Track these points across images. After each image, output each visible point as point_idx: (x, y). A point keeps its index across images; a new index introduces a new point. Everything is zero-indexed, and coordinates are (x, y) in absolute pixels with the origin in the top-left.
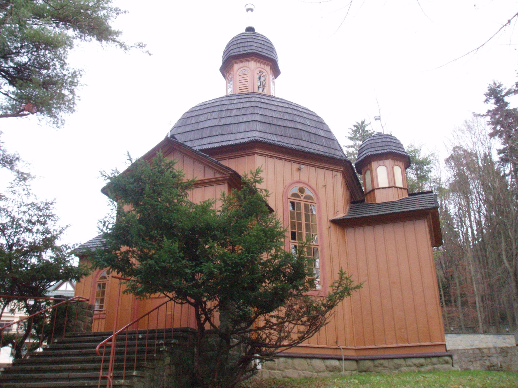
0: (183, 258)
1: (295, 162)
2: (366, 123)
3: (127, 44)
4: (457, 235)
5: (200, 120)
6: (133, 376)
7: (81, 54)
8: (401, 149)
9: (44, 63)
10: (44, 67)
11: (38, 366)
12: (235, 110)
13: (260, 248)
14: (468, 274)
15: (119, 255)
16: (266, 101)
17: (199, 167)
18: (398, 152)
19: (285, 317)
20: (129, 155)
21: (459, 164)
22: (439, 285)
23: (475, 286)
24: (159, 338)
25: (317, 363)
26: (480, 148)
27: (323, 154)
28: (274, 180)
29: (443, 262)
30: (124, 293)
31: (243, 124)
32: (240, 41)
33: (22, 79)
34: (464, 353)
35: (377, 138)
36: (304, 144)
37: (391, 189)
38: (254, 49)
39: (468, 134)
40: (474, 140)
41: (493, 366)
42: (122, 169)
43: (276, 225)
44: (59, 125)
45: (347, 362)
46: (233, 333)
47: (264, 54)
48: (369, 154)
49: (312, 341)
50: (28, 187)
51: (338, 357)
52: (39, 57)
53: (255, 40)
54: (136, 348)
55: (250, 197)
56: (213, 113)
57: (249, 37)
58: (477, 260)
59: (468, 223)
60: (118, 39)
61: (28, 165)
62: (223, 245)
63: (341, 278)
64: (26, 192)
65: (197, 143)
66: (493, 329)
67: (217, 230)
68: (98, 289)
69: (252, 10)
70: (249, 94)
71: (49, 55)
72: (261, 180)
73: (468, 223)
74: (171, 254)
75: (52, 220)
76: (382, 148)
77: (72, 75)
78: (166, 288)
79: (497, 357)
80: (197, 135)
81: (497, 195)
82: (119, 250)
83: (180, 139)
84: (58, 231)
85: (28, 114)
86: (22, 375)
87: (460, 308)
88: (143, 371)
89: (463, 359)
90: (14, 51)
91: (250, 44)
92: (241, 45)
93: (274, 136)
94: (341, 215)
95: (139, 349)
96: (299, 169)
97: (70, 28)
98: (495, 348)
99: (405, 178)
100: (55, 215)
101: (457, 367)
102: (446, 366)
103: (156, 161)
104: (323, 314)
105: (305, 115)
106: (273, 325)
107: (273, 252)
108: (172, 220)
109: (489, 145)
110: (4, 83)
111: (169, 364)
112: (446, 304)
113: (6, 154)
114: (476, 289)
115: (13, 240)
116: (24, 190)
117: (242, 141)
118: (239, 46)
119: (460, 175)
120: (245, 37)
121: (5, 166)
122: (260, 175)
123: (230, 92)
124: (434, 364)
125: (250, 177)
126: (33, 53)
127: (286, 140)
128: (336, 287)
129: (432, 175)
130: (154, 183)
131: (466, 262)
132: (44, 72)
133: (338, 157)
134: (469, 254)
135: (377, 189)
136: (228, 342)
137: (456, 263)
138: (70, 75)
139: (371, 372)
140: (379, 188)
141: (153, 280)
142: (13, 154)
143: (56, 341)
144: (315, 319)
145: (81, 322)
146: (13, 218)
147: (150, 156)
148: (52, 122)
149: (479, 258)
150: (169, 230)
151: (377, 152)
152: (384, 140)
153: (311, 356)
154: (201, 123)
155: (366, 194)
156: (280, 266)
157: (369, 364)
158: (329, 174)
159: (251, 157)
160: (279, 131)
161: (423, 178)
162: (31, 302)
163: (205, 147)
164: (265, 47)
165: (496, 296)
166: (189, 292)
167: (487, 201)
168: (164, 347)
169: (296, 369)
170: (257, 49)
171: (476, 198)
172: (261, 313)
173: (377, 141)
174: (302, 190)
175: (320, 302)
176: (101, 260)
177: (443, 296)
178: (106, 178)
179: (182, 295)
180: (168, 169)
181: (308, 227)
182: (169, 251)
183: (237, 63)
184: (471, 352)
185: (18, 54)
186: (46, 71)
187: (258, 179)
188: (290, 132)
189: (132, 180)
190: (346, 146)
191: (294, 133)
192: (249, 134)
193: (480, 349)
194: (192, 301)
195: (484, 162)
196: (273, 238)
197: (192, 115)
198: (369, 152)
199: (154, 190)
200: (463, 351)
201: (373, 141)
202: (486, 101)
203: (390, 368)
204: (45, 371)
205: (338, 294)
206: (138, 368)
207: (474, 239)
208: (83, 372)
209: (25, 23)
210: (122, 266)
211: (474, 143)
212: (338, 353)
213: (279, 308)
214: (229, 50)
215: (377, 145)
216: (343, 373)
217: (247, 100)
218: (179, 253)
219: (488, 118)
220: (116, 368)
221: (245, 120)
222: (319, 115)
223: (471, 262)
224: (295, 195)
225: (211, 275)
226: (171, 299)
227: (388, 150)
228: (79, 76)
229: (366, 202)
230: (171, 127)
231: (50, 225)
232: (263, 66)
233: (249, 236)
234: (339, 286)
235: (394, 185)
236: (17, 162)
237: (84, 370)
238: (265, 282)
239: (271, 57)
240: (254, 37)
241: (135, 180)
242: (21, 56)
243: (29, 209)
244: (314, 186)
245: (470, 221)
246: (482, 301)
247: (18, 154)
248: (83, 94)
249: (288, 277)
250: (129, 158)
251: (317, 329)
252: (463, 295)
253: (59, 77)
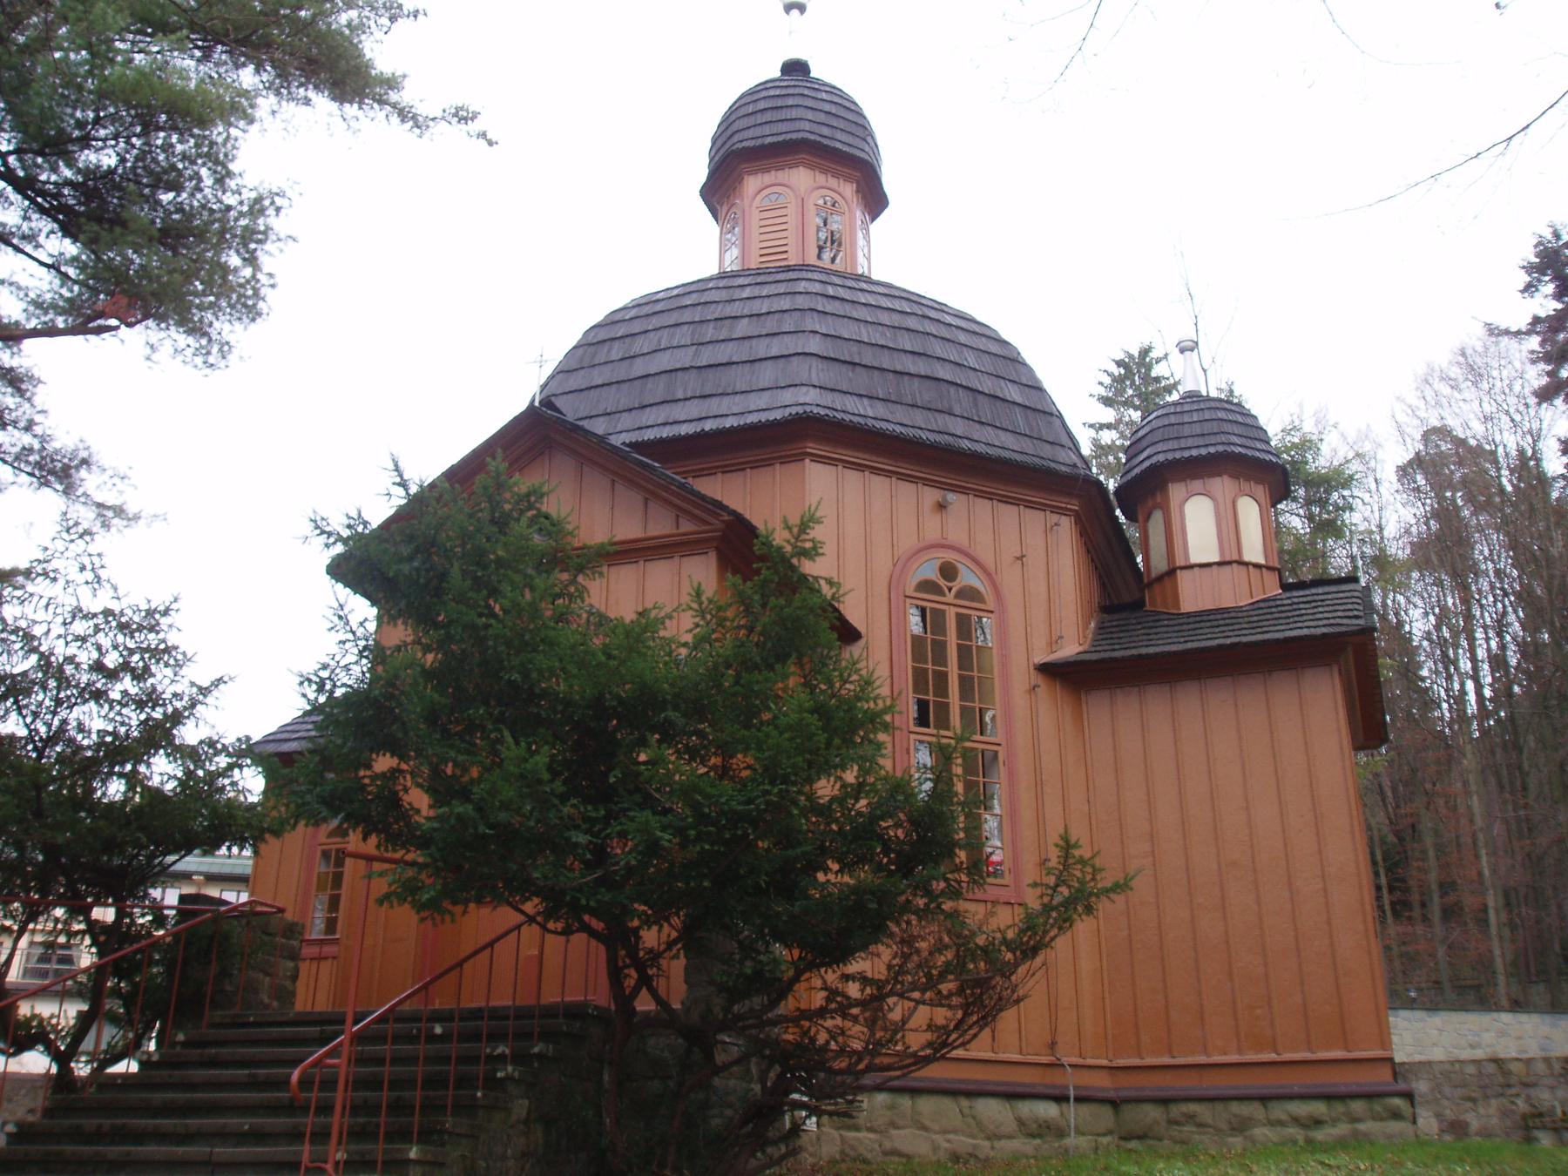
0: (564, 798)
2: (1154, 354)
3: (422, 110)
4: (1432, 704)
5: (636, 349)
6: (410, 1161)
7: (281, 145)
8: (1259, 445)
9: (165, 172)
10: (167, 182)
11: (118, 1122)
12: (746, 320)
13: (810, 767)
14: (1463, 821)
15: (367, 781)
16: (842, 293)
17: (630, 499)
18: (1250, 453)
19: (887, 982)
20: (397, 469)
21: (1439, 484)
22: (1372, 854)
23: (1484, 859)
24: (496, 1037)
25: (991, 1109)
26: (1506, 434)
27: (1018, 457)
28: (858, 536)
29: (1386, 783)
30: (380, 902)
31: (769, 363)
32: (762, 105)
33: (99, 220)
34: (1450, 1074)
35: (1186, 408)
36: (958, 427)
37: (1227, 569)
38: (805, 129)
39: (1470, 393)
40: (1487, 408)
41: (1541, 1115)
42: (378, 513)
43: (862, 690)
44: (211, 360)
45: (1086, 1110)
46: (723, 1027)
47: (838, 145)
48: (1161, 458)
49: (980, 1048)
50: (96, 560)
51: (1057, 1092)
52: (150, 152)
53: (810, 103)
54: (420, 1070)
55: (782, 601)
56: (678, 330)
57: (791, 91)
58: (1492, 780)
59: (1465, 665)
60: (393, 96)
61: (116, 480)
62: (693, 754)
63: (1066, 866)
64: (89, 576)
65: (626, 421)
66: (1539, 992)
67: (676, 708)
68: (321, 867)
69: (802, 8)
70: (789, 269)
71: (179, 148)
72: (815, 548)
73: (1465, 665)
74: (528, 786)
75: (167, 665)
76: (1201, 441)
77: (251, 207)
78: (514, 888)
79: (1552, 1088)
80: (623, 397)
81: (1556, 582)
82: (369, 767)
83: (570, 409)
84: (186, 698)
85: (116, 328)
86: (69, 1149)
87: (1438, 929)
88: (443, 1145)
89: (1447, 1090)
90: (76, 133)
91: (794, 113)
92: (768, 116)
93: (866, 401)
94: (1070, 649)
95: (433, 1066)
96: (941, 507)
97: (244, 65)
98: (1547, 1060)
99: (1273, 532)
100: (176, 648)
101: (1427, 1122)
102: (1394, 1126)
103: (485, 488)
104: (1007, 971)
105: (962, 338)
106: (851, 1006)
107: (850, 776)
108: (534, 675)
109: (1535, 426)
110: (45, 230)
111: (526, 1122)
112: (1394, 911)
113: (50, 447)
114: (1489, 870)
115: (49, 726)
116: (83, 568)
117: (764, 417)
118: (760, 119)
119: (1444, 514)
120: (778, 92)
121: (47, 484)
122: (812, 534)
123: (732, 261)
124: (1356, 1120)
125: (780, 538)
126: (134, 140)
127: (901, 414)
128: (1047, 886)
129: (1356, 519)
130: (479, 558)
131: (1459, 785)
132: (166, 197)
133: (1064, 469)
134: (1469, 762)
135: (1182, 568)
136: (709, 1056)
137: (1428, 786)
138: (245, 208)
139: (1160, 1139)
140: (1192, 567)
141: (469, 864)
142: (71, 447)
143: (181, 1037)
144: (981, 984)
145: (261, 975)
146: (45, 658)
147: (464, 474)
148: (189, 352)
149: (1497, 774)
150: (522, 707)
151: (1186, 454)
152: (1207, 415)
153: (972, 1087)
154: (639, 361)
155: (1150, 584)
156: (873, 819)
157: (1153, 1113)
158: (1035, 520)
159: (793, 467)
160: (881, 386)
161: (1329, 527)
162: (105, 914)
163: (650, 435)
165: (1550, 892)
166: (583, 902)
167: (1524, 597)
168: (510, 1068)
169: (924, 1128)
170: (815, 128)
171: (1492, 587)
172: (812, 966)
173: (1186, 419)
174: (948, 571)
175: (998, 935)
176: (308, 798)
177: (1385, 891)
178: (332, 540)
179: (563, 908)
180: (522, 512)
181: (966, 685)
182: (522, 776)
183: (751, 173)
184: (1471, 1069)
185: (85, 142)
186: (171, 195)
187: (808, 545)
188: (912, 389)
189: (405, 550)
190: (1091, 426)
191: (925, 394)
192: (788, 397)
193: (1496, 1061)
194: (597, 925)
195: (1519, 479)
196: (854, 732)
197: (612, 335)
198: (1159, 454)
199: (476, 579)
200: (1447, 1067)
201: (1173, 419)
202: (1529, 288)
203: (1218, 1131)
204: (140, 1137)
205: (1053, 909)
206: (425, 1136)
207: (1483, 713)
208: (256, 1145)
209: (111, 48)
210: (380, 814)
211: (1487, 419)
212: (1054, 1079)
213: (872, 948)
214: (729, 132)
215: (1187, 430)
216: (1071, 1141)
217: (782, 288)
218: (552, 781)
219: (1534, 342)
220: (357, 1135)
221: (774, 352)
222: (1005, 336)
223: (1473, 788)
224: (927, 586)
225: (652, 848)
226: (531, 920)
227: (1221, 448)
228: (271, 211)
229: (1148, 607)
230: (549, 370)
231: (161, 677)
232: (833, 182)
233: (776, 727)
234: (1057, 886)
235: (1235, 557)
236: (83, 473)
237: (258, 1136)
238: (826, 870)
239: (862, 155)
240: (806, 92)
241: (417, 551)
242: (98, 150)
243: (97, 629)
244: (987, 558)
245: (1474, 659)
246: (1508, 904)
247: (87, 448)
248: (285, 266)
249: (898, 854)
250: (398, 480)
251: (988, 1020)
252: (1446, 887)
253: (212, 211)
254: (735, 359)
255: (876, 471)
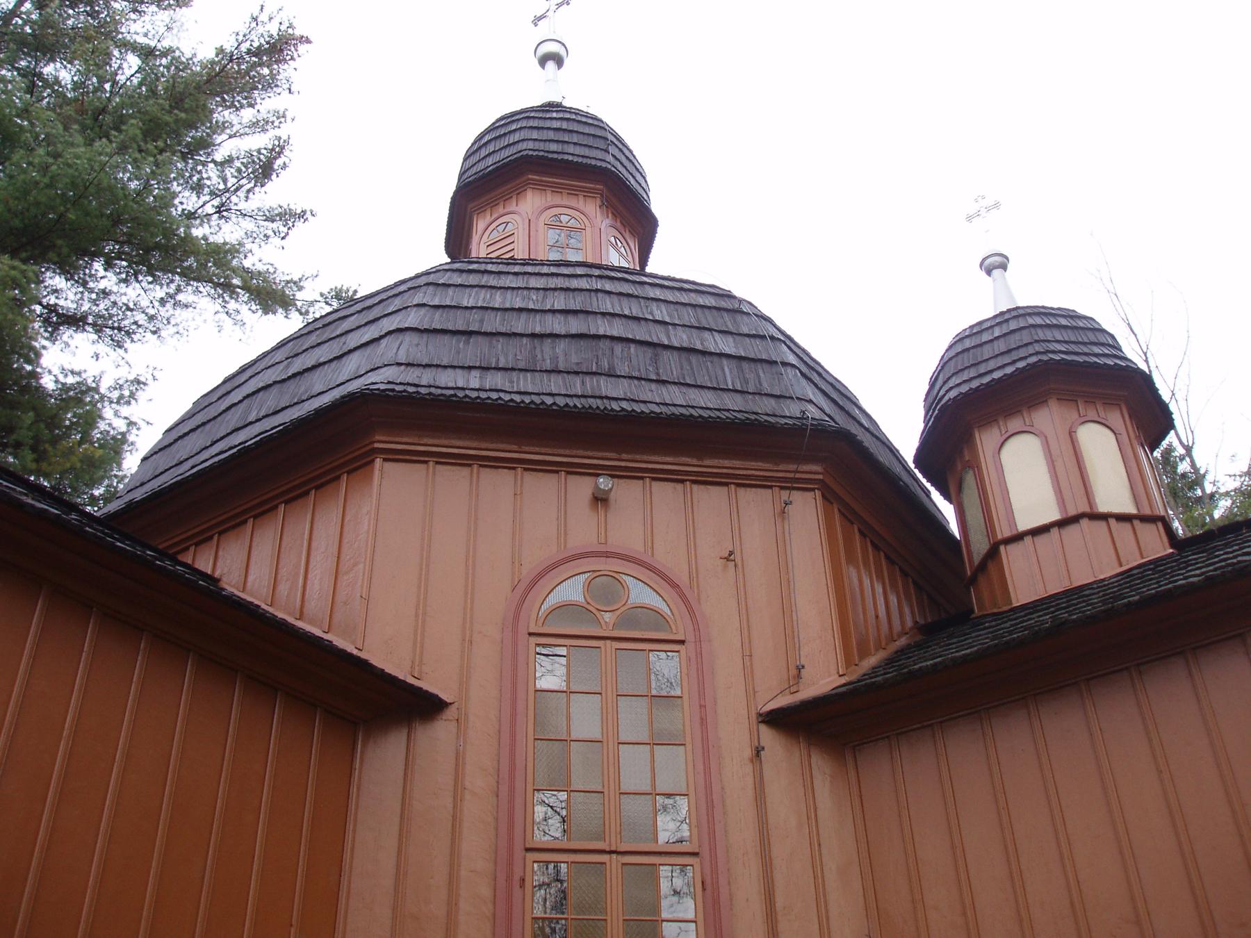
1: (573, 470)
37: (1072, 530)
69: (559, 60)
76: (1007, 359)
140: (1019, 537)
158: (755, 506)
164: (575, 138)
215: (987, 352)
235: (1084, 508)
254: (322, 360)
255: (444, 459)
